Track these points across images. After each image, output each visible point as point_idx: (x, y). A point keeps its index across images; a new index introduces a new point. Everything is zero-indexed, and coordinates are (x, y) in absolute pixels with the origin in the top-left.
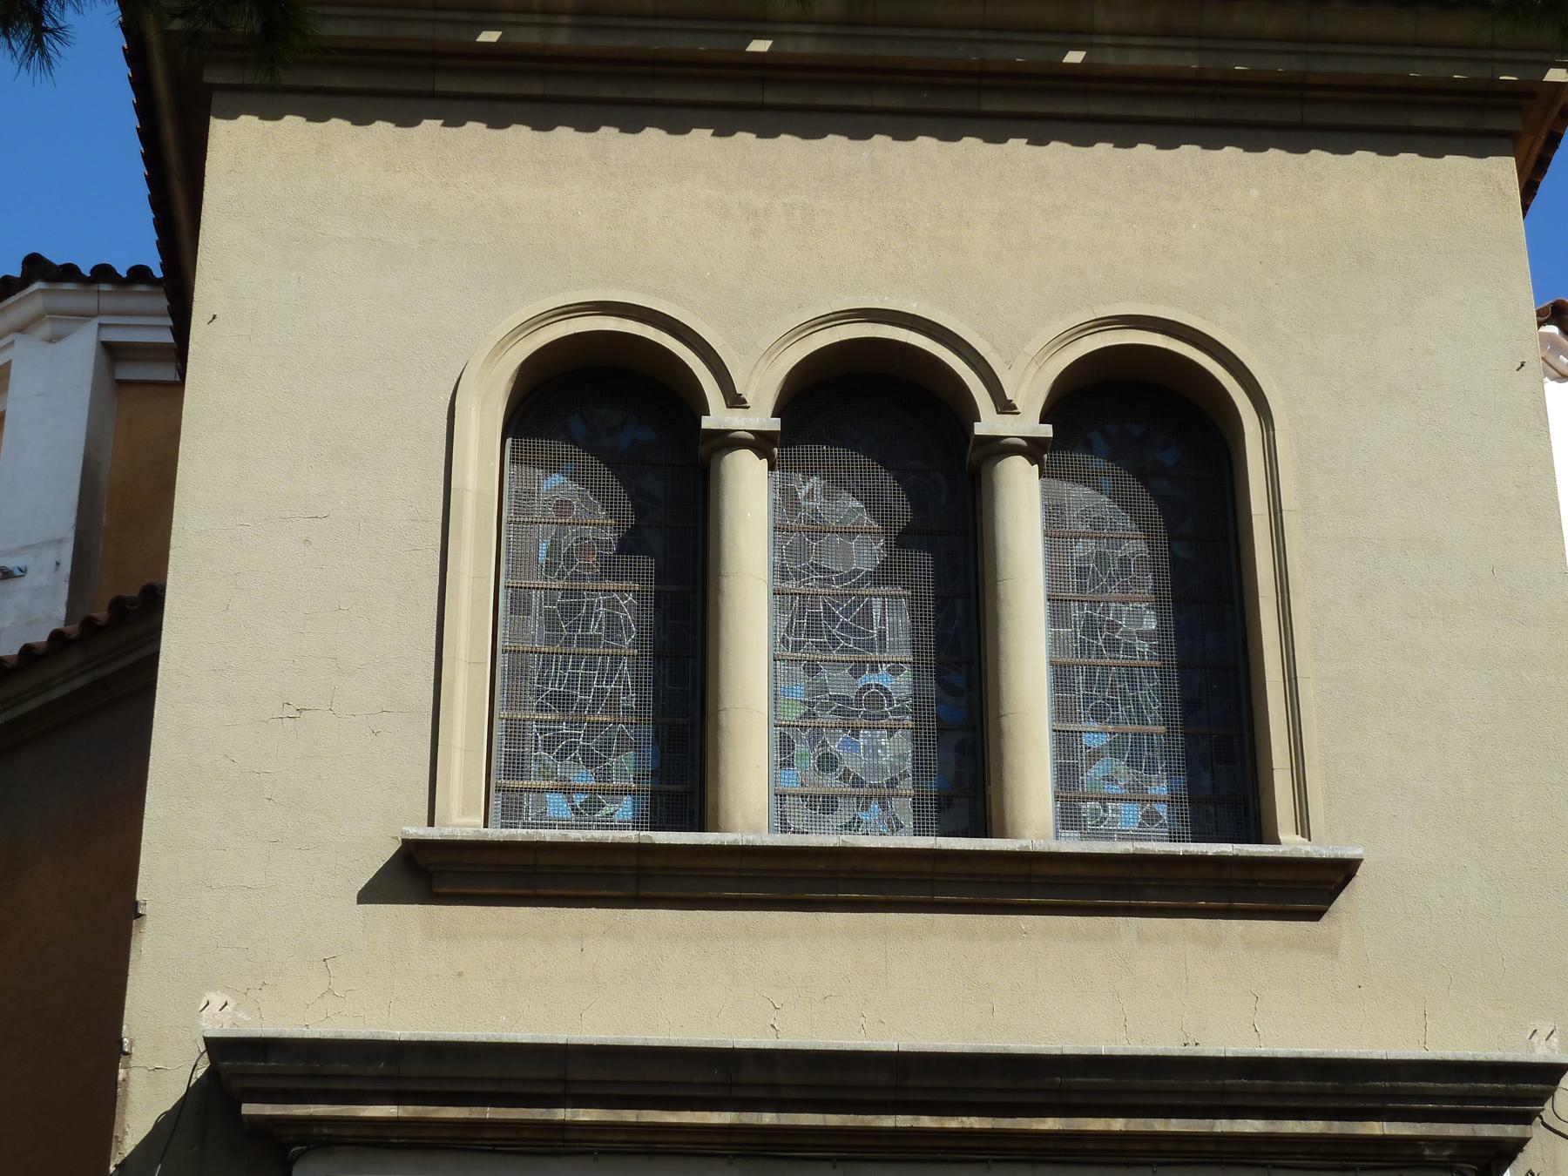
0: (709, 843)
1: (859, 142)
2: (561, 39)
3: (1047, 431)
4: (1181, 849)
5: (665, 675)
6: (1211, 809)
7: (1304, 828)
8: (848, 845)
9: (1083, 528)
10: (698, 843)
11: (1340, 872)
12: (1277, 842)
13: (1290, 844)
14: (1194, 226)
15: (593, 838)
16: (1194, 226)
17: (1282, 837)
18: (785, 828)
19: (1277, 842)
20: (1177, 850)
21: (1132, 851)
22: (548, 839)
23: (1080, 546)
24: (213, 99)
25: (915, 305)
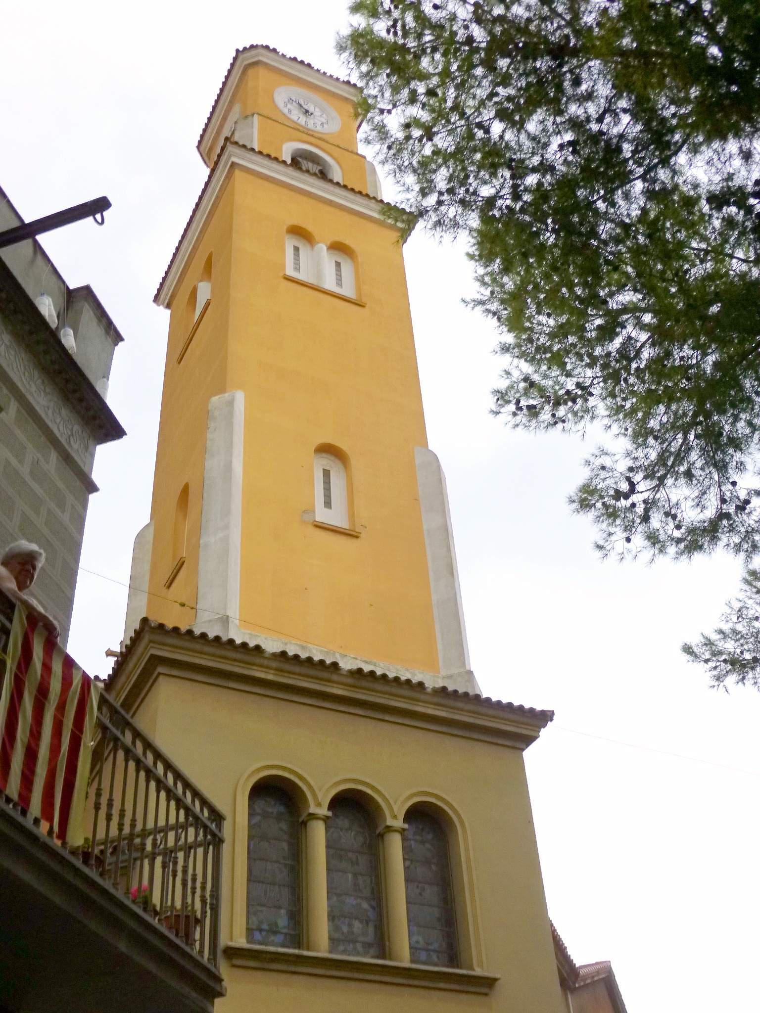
2: (270, 677)
3: (330, 814)
7: (481, 966)
13: (478, 972)
19: (473, 970)
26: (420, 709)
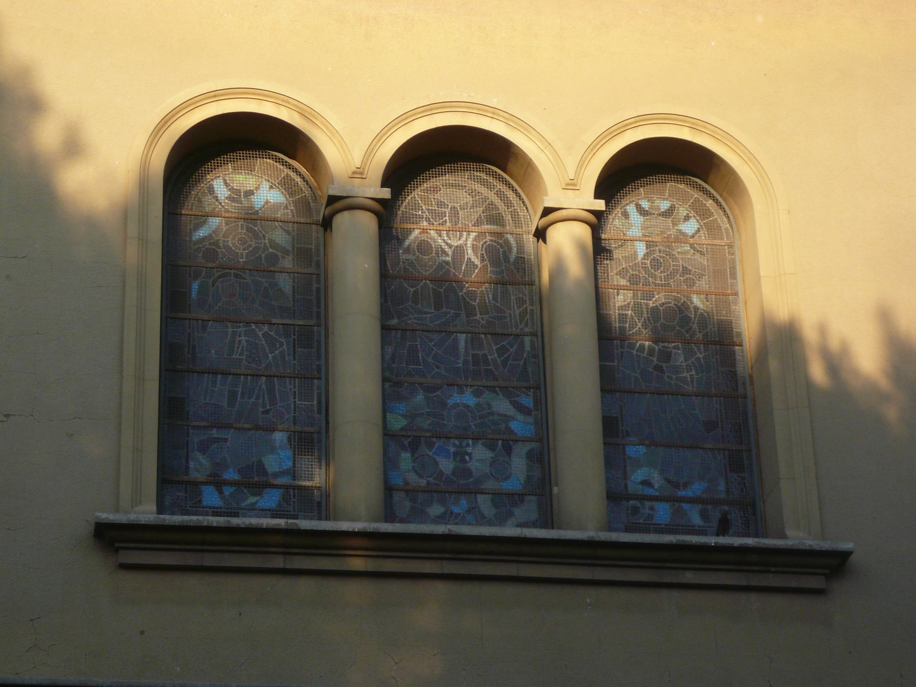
0: (343, 529)
1: (606, 160)
4: (713, 541)
5: (295, 392)
6: (457, 442)
8: (453, 533)
9: (623, 282)
10: (335, 529)
12: (784, 536)
14: (713, 44)
15: (251, 524)
16: (713, 44)
17: (789, 533)
18: (389, 517)
19: (784, 536)
20: (710, 542)
21: (674, 542)
22: (215, 524)
23: (621, 297)
24: (379, 205)
25: (495, 100)
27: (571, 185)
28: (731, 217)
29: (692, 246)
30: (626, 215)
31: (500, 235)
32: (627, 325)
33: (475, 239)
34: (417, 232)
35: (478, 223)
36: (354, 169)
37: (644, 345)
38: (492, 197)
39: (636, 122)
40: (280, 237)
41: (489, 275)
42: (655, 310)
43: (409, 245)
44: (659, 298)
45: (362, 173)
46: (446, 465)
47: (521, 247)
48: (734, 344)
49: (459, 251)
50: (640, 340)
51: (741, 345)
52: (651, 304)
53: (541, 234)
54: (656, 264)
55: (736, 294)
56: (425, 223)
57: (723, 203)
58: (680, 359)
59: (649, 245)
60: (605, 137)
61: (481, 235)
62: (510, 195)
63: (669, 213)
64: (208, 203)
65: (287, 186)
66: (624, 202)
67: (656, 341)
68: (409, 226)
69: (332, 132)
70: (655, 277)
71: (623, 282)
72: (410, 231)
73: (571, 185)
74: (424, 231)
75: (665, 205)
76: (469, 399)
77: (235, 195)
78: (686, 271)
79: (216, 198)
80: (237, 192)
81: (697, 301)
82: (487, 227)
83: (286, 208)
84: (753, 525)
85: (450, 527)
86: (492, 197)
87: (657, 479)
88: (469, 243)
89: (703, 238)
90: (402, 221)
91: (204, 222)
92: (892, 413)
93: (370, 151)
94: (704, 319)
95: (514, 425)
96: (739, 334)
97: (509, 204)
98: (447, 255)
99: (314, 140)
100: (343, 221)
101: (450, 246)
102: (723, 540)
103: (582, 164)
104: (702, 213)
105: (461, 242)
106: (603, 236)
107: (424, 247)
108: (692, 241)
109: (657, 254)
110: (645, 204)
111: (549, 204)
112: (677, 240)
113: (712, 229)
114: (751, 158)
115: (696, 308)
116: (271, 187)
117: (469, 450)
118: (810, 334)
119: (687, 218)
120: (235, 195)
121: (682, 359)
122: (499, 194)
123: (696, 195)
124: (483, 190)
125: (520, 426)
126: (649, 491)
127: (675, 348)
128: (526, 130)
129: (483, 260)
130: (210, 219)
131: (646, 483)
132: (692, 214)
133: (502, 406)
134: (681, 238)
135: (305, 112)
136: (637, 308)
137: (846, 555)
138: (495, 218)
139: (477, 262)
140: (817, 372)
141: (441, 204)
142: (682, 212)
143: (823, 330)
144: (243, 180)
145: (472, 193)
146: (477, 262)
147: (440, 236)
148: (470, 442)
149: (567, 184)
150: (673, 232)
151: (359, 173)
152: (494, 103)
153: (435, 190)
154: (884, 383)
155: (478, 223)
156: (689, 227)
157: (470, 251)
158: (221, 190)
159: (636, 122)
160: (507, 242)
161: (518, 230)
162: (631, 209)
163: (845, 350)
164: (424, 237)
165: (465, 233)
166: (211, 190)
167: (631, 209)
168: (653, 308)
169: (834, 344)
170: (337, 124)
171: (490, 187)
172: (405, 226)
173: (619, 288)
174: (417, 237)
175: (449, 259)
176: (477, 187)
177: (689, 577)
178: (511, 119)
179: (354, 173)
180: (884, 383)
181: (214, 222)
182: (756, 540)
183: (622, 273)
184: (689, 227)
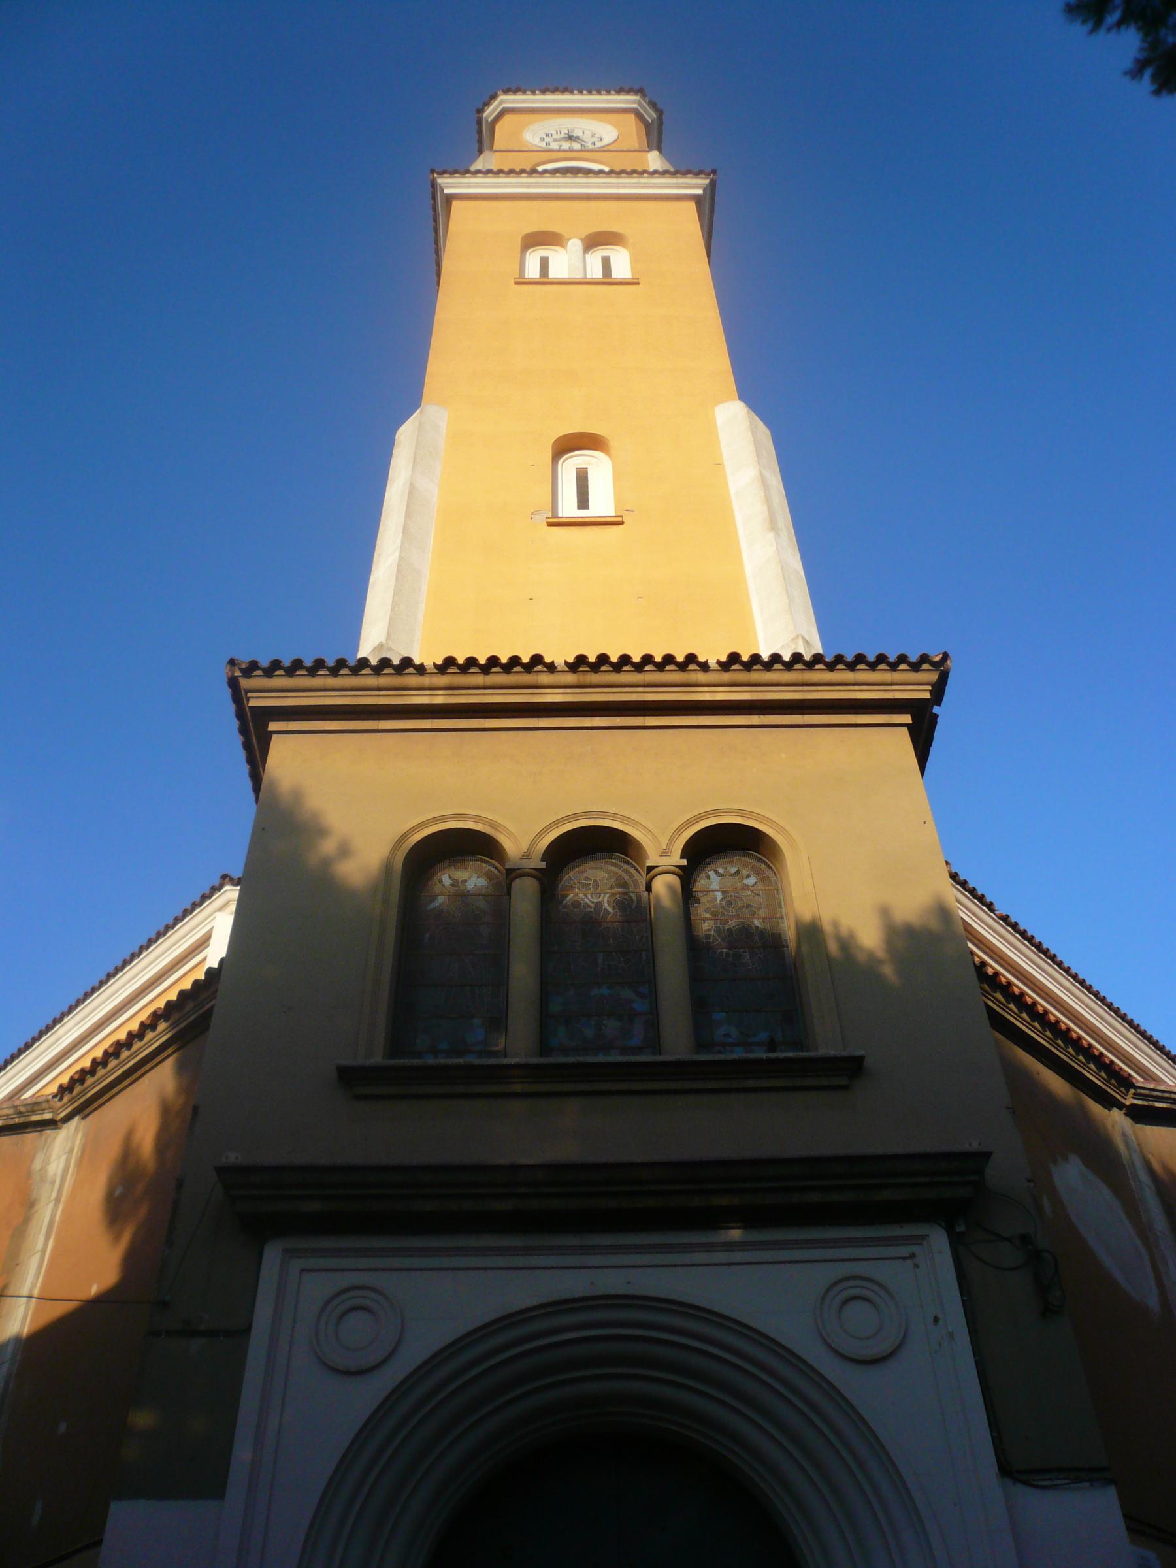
3: (684, 862)
9: (708, 915)
11: (853, 1067)
23: (706, 925)
26: (705, 695)
27: (665, 853)
28: (776, 872)
29: (752, 891)
30: (708, 877)
31: (625, 894)
32: (711, 941)
33: (610, 897)
34: (571, 896)
35: (612, 887)
36: (523, 853)
37: (723, 952)
38: (620, 872)
39: (706, 815)
40: (482, 904)
41: (618, 917)
42: (730, 930)
43: (566, 903)
44: (732, 923)
45: (528, 856)
46: (589, 1033)
47: (639, 899)
48: (784, 946)
49: (599, 905)
50: (719, 948)
51: (787, 947)
52: (726, 927)
53: (649, 888)
54: (729, 903)
55: (782, 917)
56: (577, 890)
57: (771, 865)
58: (747, 957)
59: (724, 893)
60: (687, 825)
61: (613, 895)
62: (632, 871)
63: (737, 874)
64: (437, 888)
65: (488, 876)
66: (707, 870)
67: (730, 948)
68: (568, 892)
69: (510, 835)
70: (728, 911)
71: (708, 915)
72: (567, 895)
73: (665, 853)
74: (576, 895)
75: (734, 870)
76: (605, 991)
77: (455, 883)
78: (749, 906)
79: (443, 885)
80: (457, 881)
81: (756, 922)
82: (616, 890)
83: (488, 888)
84: (799, 1045)
85: (578, 1058)
86: (620, 872)
87: (734, 1032)
88: (606, 899)
89: (760, 886)
90: (562, 890)
91: (435, 900)
92: (888, 970)
93: (534, 842)
94: (762, 933)
95: (635, 1006)
96: (786, 941)
97: (631, 876)
98: (591, 907)
99: (499, 840)
100: (517, 884)
101: (593, 902)
102: (772, 1055)
103: (671, 841)
104: (758, 872)
105: (600, 899)
106: (694, 890)
107: (576, 904)
108: (752, 889)
109: (729, 899)
110: (721, 870)
111: (649, 863)
112: (743, 889)
113: (765, 881)
114: (782, 830)
115: (757, 927)
116: (478, 877)
117: (605, 1022)
118: (827, 927)
119: (748, 876)
120: (455, 883)
121: (748, 957)
122: (626, 871)
123: (754, 862)
124: (614, 869)
125: (639, 1005)
126: (730, 1040)
127: (743, 952)
128: (635, 824)
129: (614, 909)
130: (439, 898)
131: (727, 1035)
132: (752, 873)
133: (627, 993)
134: (745, 887)
135: (492, 824)
136: (718, 930)
137: (861, 1059)
138: (624, 885)
139: (610, 910)
140: (833, 947)
141: (586, 879)
142: (745, 873)
143: (835, 924)
144: (460, 874)
145: (609, 872)
146: (610, 910)
147: (587, 897)
148: (605, 1017)
149: (662, 853)
150: (739, 884)
151: (527, 855)
152: (614, 810)
153: (583, 871)
154: (881, 954)
155: (612, 887)
156: (751, 881)
157: (606, 904)
158: (446, 880)
159: (706, 815)
160: (631, 898)
161: (637, 891)
162: (712, 874)
163: (852, 935)
164: (576, 898)
165: (602, 895)
166: (440, 881)
167: (712, 874)
168: (728, 929)
169: (844, 932)
170: (512, 829)
171: (615, 865)
172: (563, 893)
173: (705, 919)
174: (571, 899)
175: (592, 910)
176: (610, 867)
177: (751, 1083)
178: (624, 819)
179: (523, 856)
180: (881, 954)
181: (441, 899)
182: (796, 1053)
183: (706, 911)
184: (751, 881)
